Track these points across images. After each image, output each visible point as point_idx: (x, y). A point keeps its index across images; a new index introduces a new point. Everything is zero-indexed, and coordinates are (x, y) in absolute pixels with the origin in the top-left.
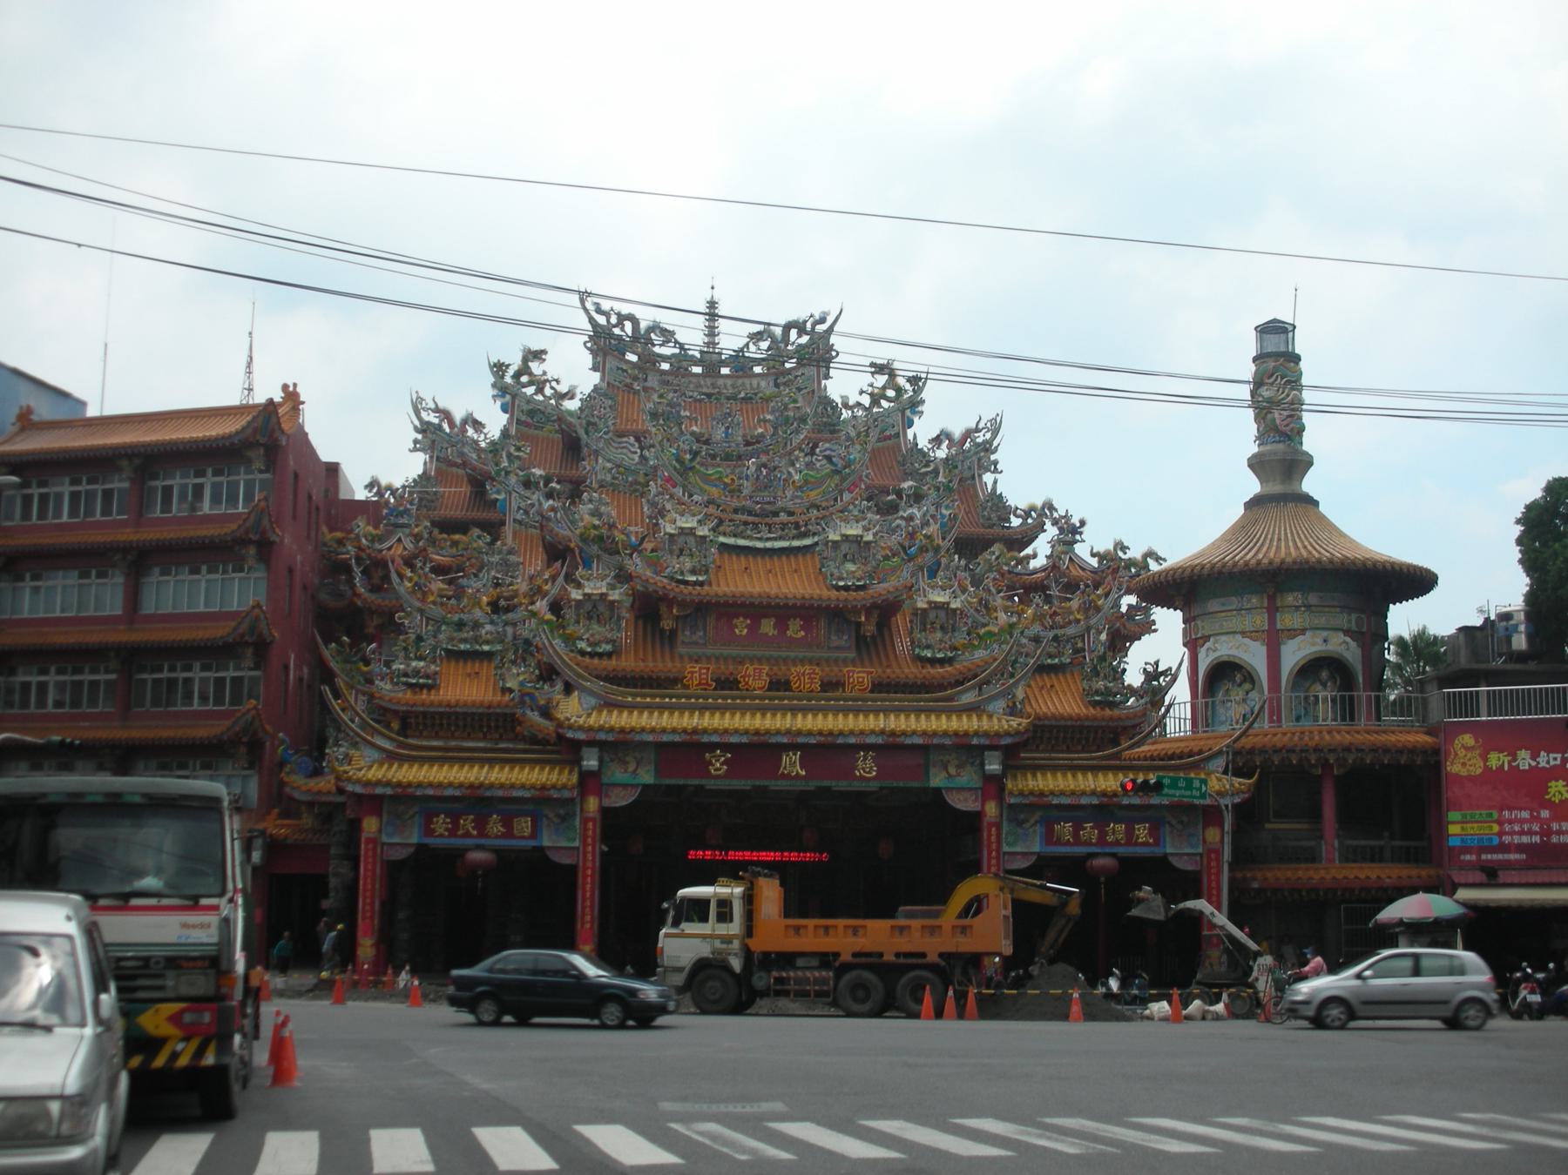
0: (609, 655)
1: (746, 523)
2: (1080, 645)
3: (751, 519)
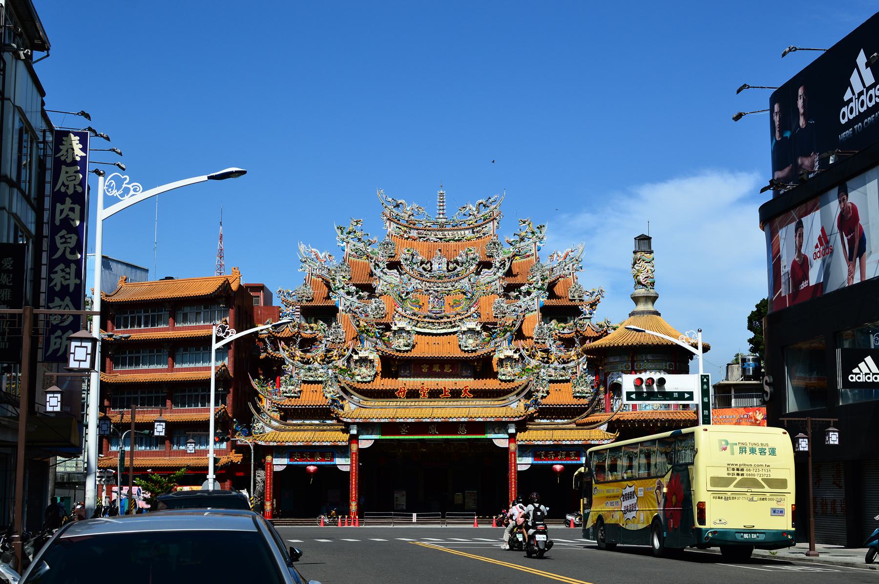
0: (369, 382)
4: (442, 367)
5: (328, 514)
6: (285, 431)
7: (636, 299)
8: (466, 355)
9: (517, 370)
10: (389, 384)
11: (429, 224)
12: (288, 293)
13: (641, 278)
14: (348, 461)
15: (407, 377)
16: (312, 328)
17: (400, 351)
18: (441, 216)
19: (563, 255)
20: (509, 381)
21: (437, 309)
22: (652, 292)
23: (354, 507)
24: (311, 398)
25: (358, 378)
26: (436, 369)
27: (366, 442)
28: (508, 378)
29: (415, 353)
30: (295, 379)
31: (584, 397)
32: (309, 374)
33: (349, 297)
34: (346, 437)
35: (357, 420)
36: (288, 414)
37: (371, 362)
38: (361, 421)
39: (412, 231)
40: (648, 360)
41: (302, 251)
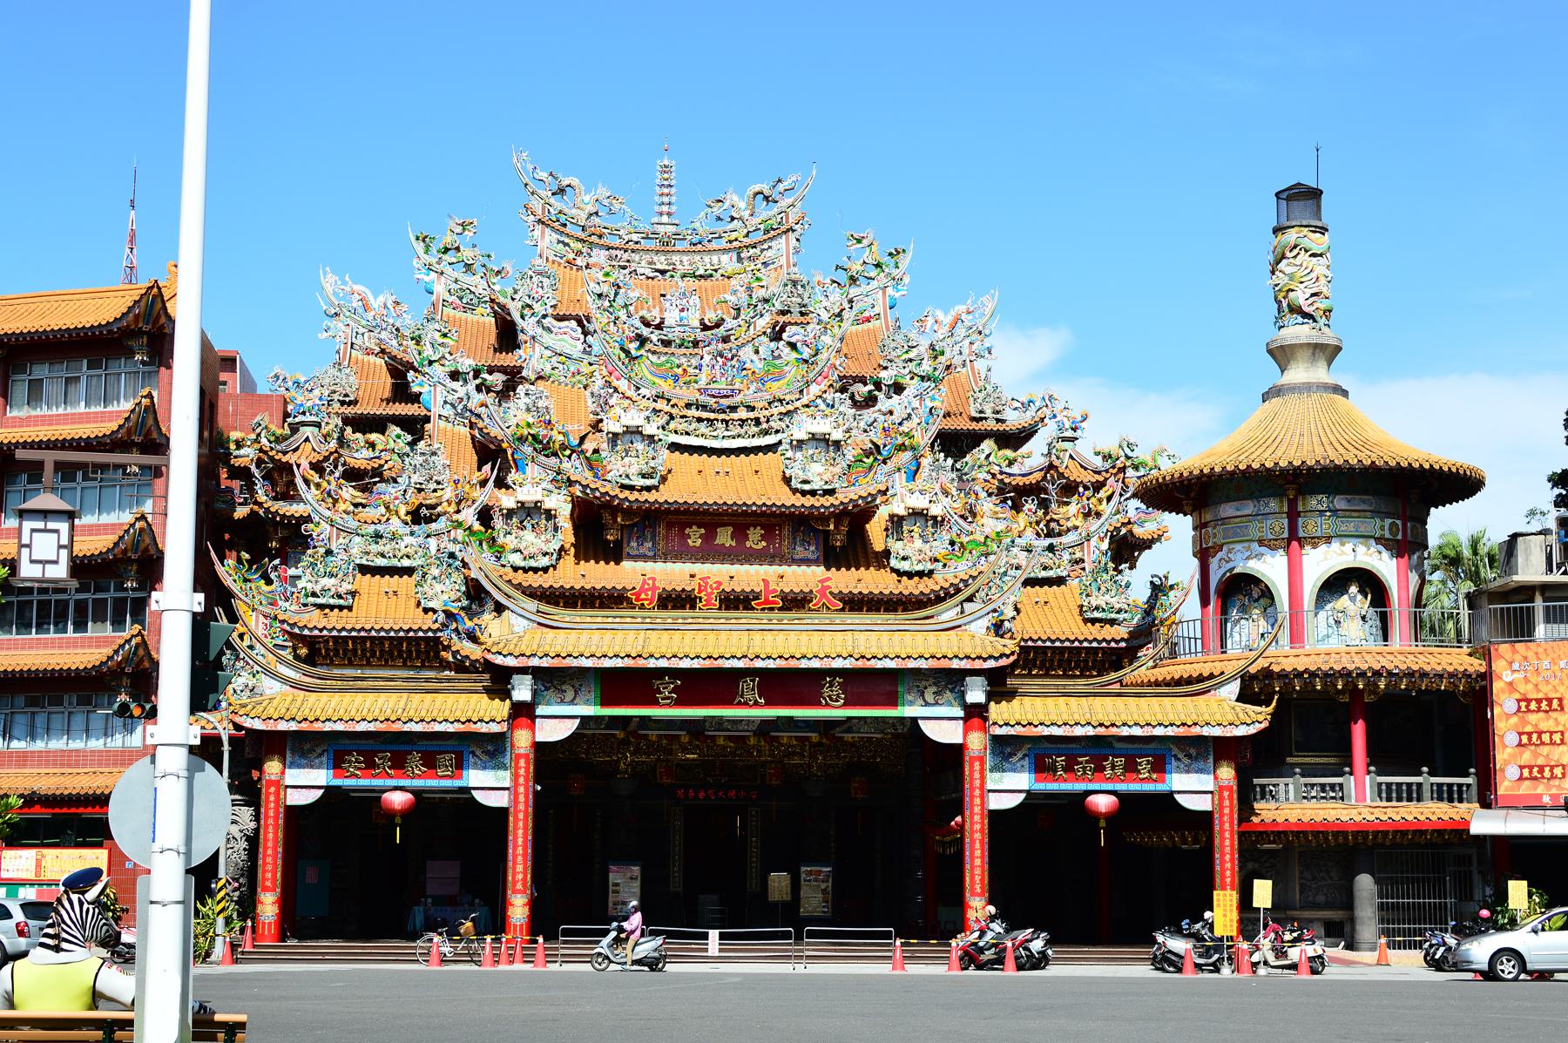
0: (545, 570)
1: (700, 420)
2: (1078, 555)
3: (705, 415)
4: (740, 533)
5: (453, 932)
6: (323, 690)
7: (1281, 355)
8: (809, 501)
9: (940, 547)
10: (599, 575)
11: (635, 237)
12: (297, 384)
13: (1300, 297)
14: (503, 778)
15: (644, 558)
16: (372, 445)
17: (631, 488)
18: (665, 219)
19: (947, 319)
20: (921, 574)
21: (721, 385)
22: (1328, 337)
23: (518, 910)
24: (384, 609)
25: (517, 559)
26: (724, 538)
27: (556, 724)
28: (919, 567)
29: (668, 494)
30: (338, 560)
31: (1112, 622)
32: (374, 548)
33: (456, 385)
34: (501, 709)
35: (535, 662)
36: (321, 653)
37: (550, 515)
38: (545, 663)
39: (595, 252)
40: (1335, 512)
41: (329, 289)
